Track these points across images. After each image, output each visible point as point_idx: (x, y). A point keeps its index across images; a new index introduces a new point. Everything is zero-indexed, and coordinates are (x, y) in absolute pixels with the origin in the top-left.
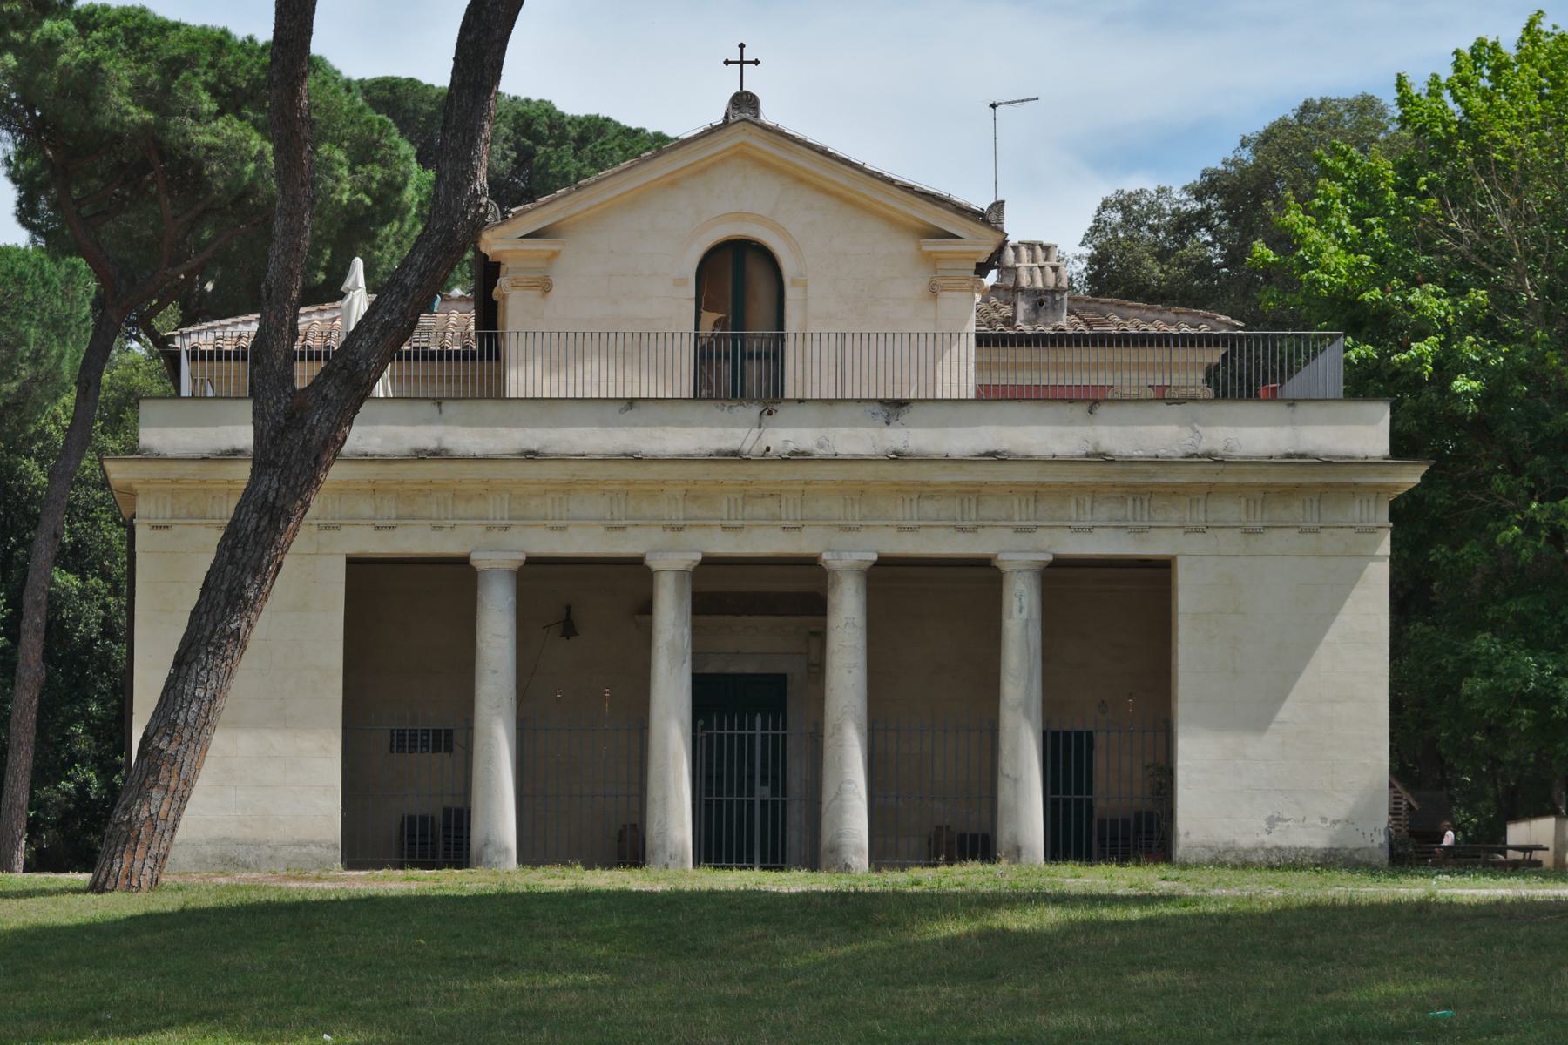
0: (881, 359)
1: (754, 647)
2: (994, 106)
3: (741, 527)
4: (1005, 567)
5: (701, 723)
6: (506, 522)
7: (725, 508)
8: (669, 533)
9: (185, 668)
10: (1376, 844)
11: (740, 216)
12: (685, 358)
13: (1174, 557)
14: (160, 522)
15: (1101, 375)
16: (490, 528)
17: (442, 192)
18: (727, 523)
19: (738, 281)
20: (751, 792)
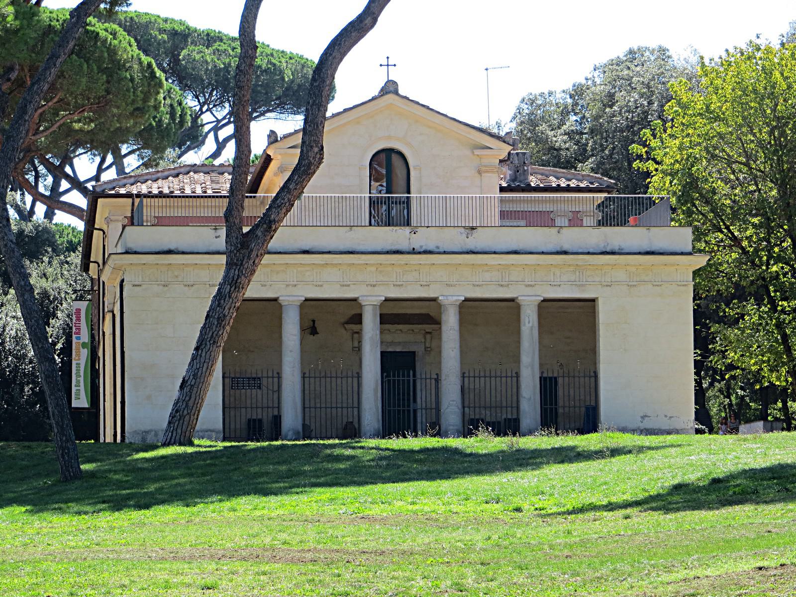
0: (456, 205)
1: (405, 338)
2: (487, 69)
3: (402, 285)
4: (522, 303)
5: (385, 374)
6: (295, 283)
7: (395, 277)
8: (370, 288)
9: (200, 351)
10: (689, 427)
11: (389, 138)
12: (415, 219)
13: (597, 298)
14: (137, 283)
15: (548, 205)
16: (287, 285)
17: (305, 149)
18: (395, 283)
19: (388, 166)
20: (409, 406)
